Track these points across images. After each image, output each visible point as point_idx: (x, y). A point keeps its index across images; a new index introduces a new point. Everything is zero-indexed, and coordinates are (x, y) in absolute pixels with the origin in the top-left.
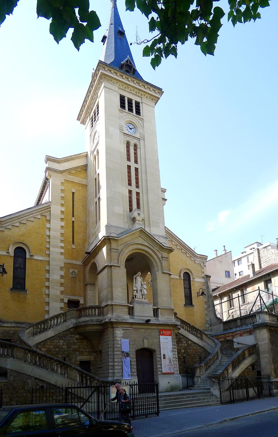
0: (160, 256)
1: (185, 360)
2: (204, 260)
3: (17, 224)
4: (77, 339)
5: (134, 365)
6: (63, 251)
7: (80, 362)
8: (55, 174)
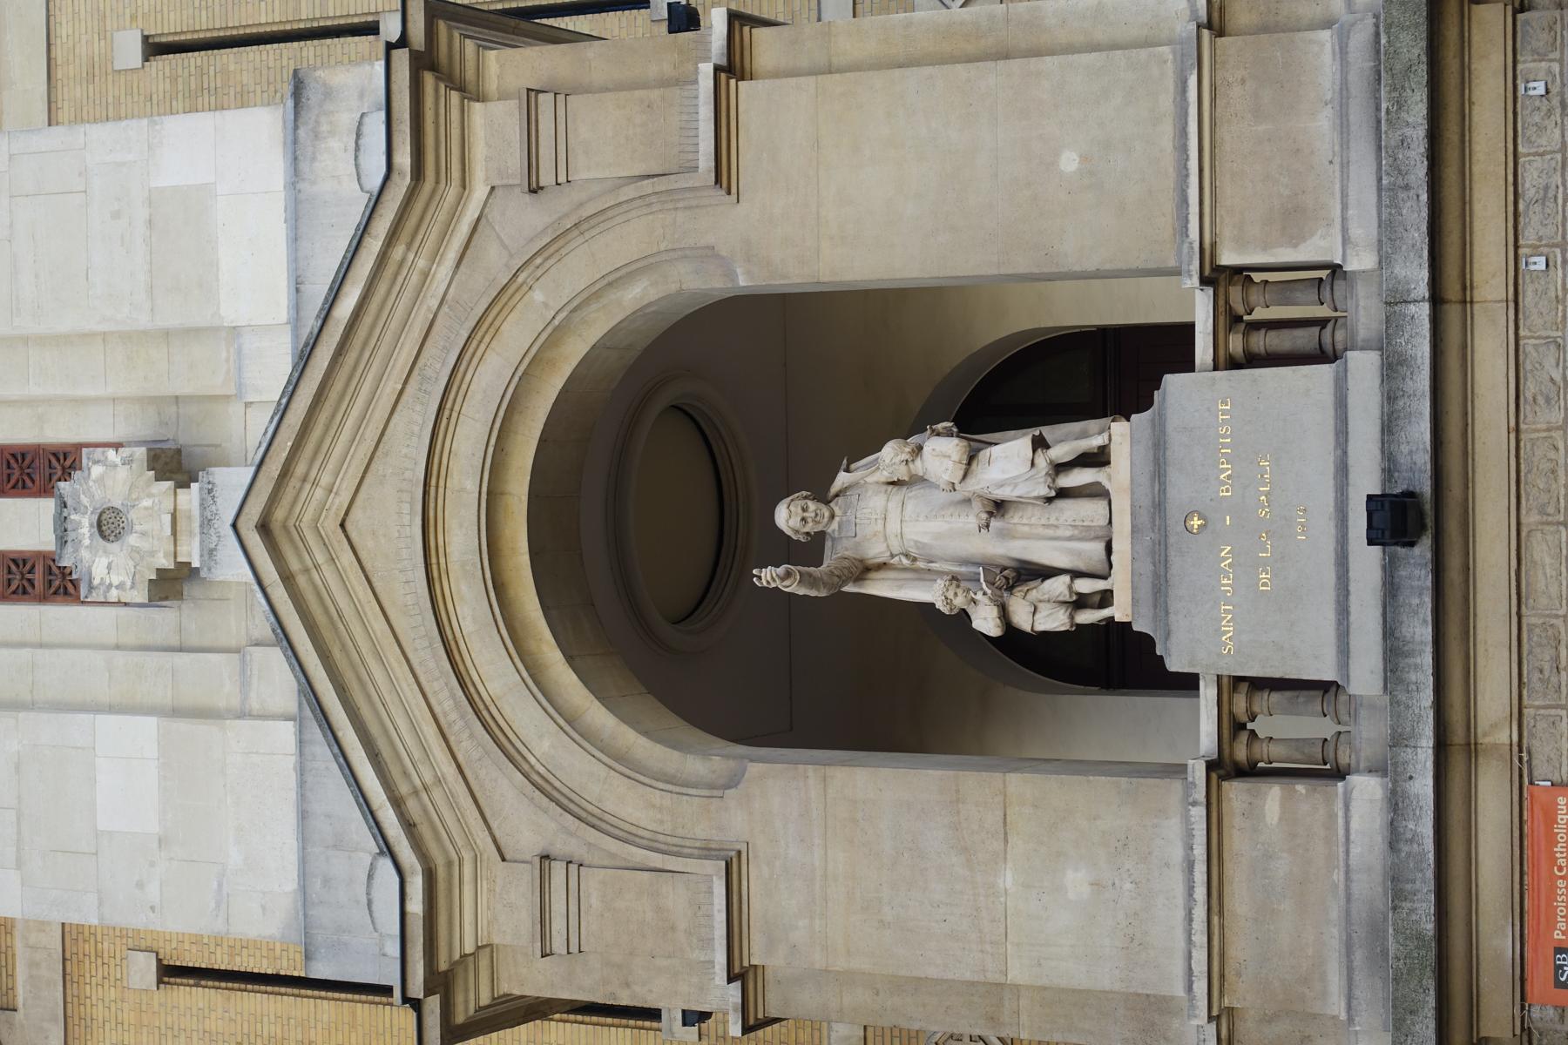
0: (523, 221)
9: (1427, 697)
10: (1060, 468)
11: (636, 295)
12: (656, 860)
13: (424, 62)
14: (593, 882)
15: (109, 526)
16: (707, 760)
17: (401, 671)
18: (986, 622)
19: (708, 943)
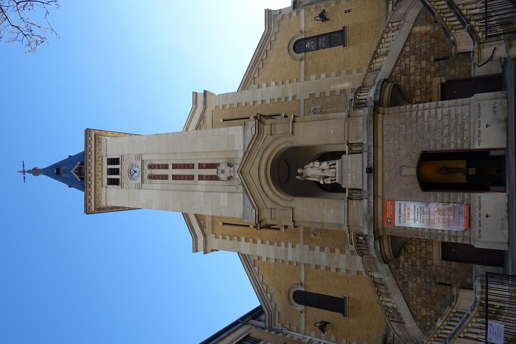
1: (442, 57)
2: (272, 16)
3: (269, 295)
4: (406, 260)
5: (450, 196)
6: (290, 245)
7: (443, 258)
8: (209, 244)
9: (372, 190)
10: (330, 165)
11: (282, 146)
12: (284, 209)
13: (259, 121)
14: (277, 211)
15: (223, 172)
16: (290, 198)
17: (255, 188)
18: (322, 182)
19: (290, 218)
